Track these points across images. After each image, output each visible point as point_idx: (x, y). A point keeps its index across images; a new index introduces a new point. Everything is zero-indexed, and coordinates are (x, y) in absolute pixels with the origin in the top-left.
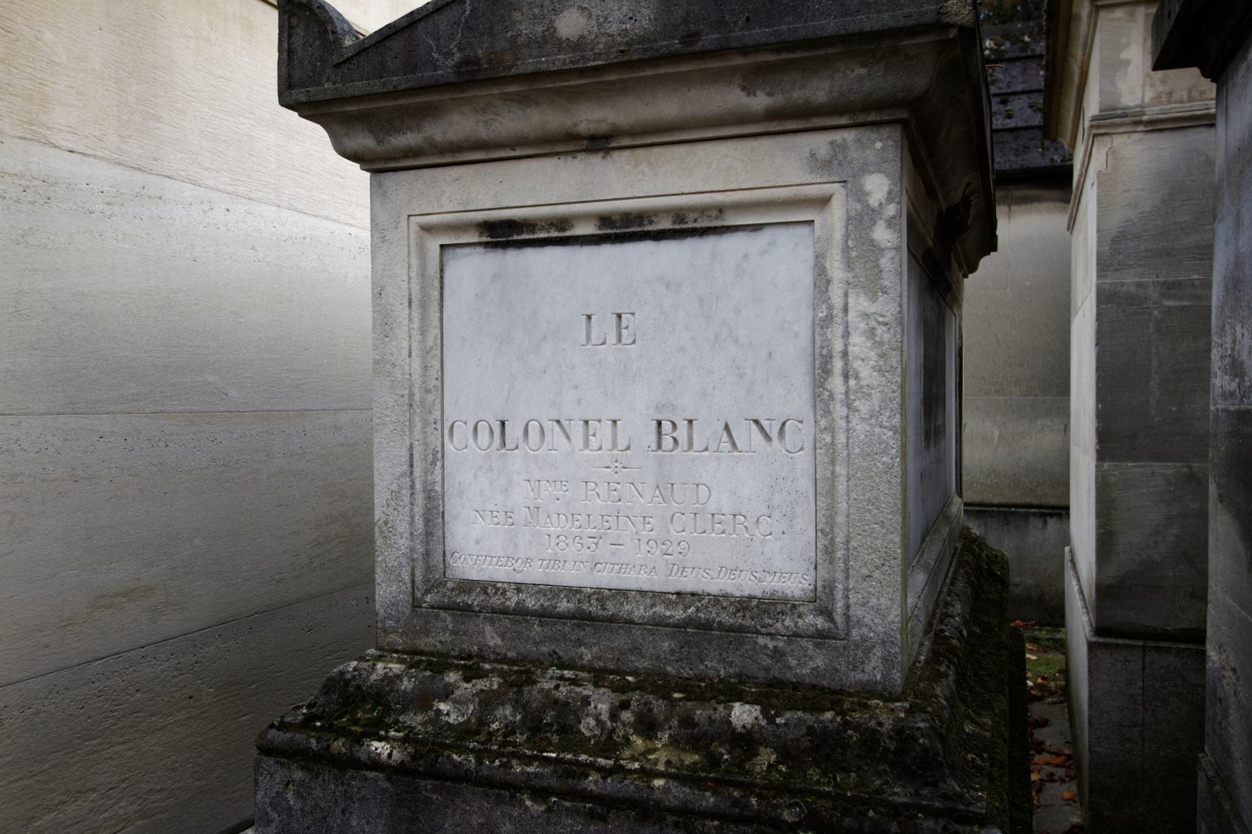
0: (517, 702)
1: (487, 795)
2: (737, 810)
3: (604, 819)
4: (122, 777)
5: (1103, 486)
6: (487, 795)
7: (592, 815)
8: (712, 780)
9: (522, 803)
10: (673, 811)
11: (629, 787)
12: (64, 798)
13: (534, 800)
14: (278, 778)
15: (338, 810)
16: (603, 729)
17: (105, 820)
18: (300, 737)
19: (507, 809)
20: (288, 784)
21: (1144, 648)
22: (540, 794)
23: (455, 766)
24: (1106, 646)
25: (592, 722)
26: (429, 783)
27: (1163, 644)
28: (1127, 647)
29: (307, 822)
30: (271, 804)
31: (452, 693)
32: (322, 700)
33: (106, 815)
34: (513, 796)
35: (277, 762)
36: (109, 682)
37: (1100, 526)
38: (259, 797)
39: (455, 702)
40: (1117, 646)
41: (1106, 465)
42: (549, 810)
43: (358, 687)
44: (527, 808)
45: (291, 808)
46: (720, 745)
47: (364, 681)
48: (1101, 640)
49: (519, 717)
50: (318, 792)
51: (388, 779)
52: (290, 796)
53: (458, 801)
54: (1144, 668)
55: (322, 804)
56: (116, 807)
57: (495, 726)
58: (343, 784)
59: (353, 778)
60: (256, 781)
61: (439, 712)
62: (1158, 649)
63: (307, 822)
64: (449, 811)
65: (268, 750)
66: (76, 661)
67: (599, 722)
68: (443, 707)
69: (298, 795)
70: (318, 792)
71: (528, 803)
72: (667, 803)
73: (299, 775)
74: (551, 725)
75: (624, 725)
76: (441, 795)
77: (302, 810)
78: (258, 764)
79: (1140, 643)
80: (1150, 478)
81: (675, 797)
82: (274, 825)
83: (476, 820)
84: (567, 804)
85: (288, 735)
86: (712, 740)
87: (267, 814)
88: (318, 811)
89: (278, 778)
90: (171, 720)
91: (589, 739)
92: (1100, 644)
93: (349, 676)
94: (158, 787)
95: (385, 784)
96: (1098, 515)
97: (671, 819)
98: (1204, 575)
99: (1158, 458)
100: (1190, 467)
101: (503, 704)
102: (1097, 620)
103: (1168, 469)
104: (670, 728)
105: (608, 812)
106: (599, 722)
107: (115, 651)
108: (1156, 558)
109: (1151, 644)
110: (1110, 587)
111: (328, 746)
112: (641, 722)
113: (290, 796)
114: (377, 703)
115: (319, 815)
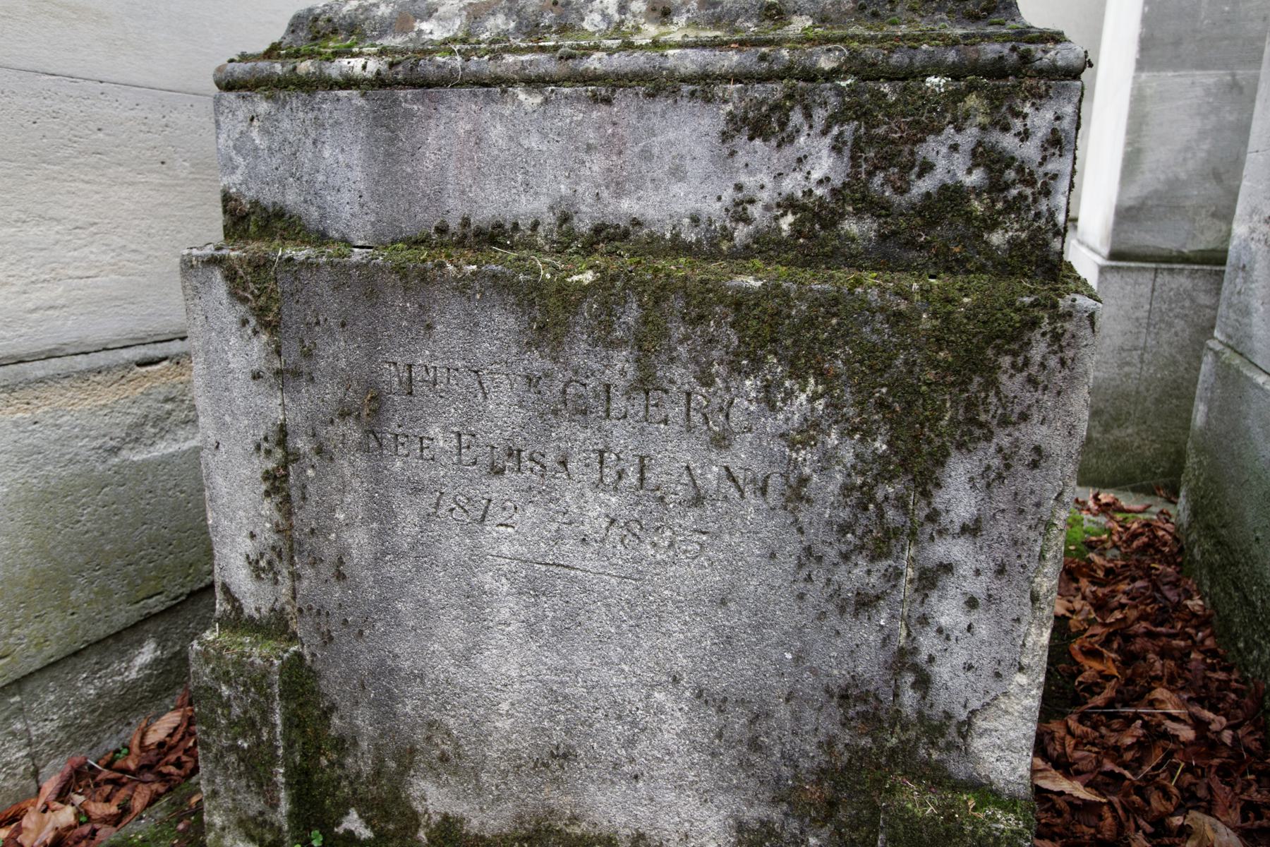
0: (510, 9)
1: (475, 95)
2: (765, 65)
3: (608, 101)
4: (92, 220)
5: (1138, 99)
6: (475, 95)
7: (595, 99)
8: (735, 42)
9: (515, 96)
10: (686, 80)
11: (637, 61)
12: (23, 217)
13: (529, 93)
14: (240, 115)
15: (309, 142)
16: (609, 23)
17: (75, 259)
18: (263, 65)
19: (496, 108)
20: (252, 119)
21: (1156, 269)
22: (535, 82)
23: (439, 67)
24: (1118, 269)
25: (597, 17)
26: (409, 93)
27: (1175, 266)
28: (1139, 269)
29: (275, 162)
30: (235, 147)
31: (436, 10)
32: (288, 39)
33: (76, 254)
34: (504, 91)
35: (238, 97)
36: (63, 106)
37: (1129, 143)
38: (221, 141)
39: (440, 19)
40: (1129, 269)
41: (1144, 76)
42: (546, 101)
43: (329, 20)
44: (521, 103)
45: (256, 149)
46: (746, 21)
47: (336, 13)
48: (1114, 263)
49: (512, 25)
50: (286, 124)
51: (363, 95)
52: (255, 134)
53: (442, 108)
54: (1153, 290)
55: (291, 138)
56: (86, 250)
57: (483, 37)
58: (312, 110)
59: (324, 100)
60: (217, 122)
61: (420, 32)
62: (1171, 270)
63: (275, 162)
64: (432, 122)
65: (229, 85)
66: (21, 65)
67: (605, 16)
68: (426, 26)
69: (264, 131)
70: (286, 124)
71: (522, 96)
72: (682, 70)
73: (263, 107)
74: (550, 27)
75: (634, 16)
76: (423, 104)
77: (270, 149)
78: (217, 101)
79: (1153, 265)
80: (1188, 87)
81: (692, 61)
82: (239, 172)
83: (463, 127)
84: (567, 90)
85: (249, 65)
86: (738, 16)
87: (231, 159)
88: (287, 146)
89: (240, 115)
90: (140, 178)
91: (594, 33)
92: (1112, 267)
93: (318, 11)
94: (133, 247)
95: (360, 102)
96: (1128, 132)
97: (686, 88)
98: (1234, 195)
99: (1202, 65)
100: (1233, 75)
101: (494, 14)
102: (1113, 242)
103: (1209, 78)
104: (688, 11)
105: (614, 91)
106: (605, 16)
107: (69, 72)
108: (1183, 176)
109: (1163, 266)
110: (1130, 209)
111: (295, 68)
112: (654, 10)
113: (255, 134)
114: (352, 33)
115: (288, 152)
